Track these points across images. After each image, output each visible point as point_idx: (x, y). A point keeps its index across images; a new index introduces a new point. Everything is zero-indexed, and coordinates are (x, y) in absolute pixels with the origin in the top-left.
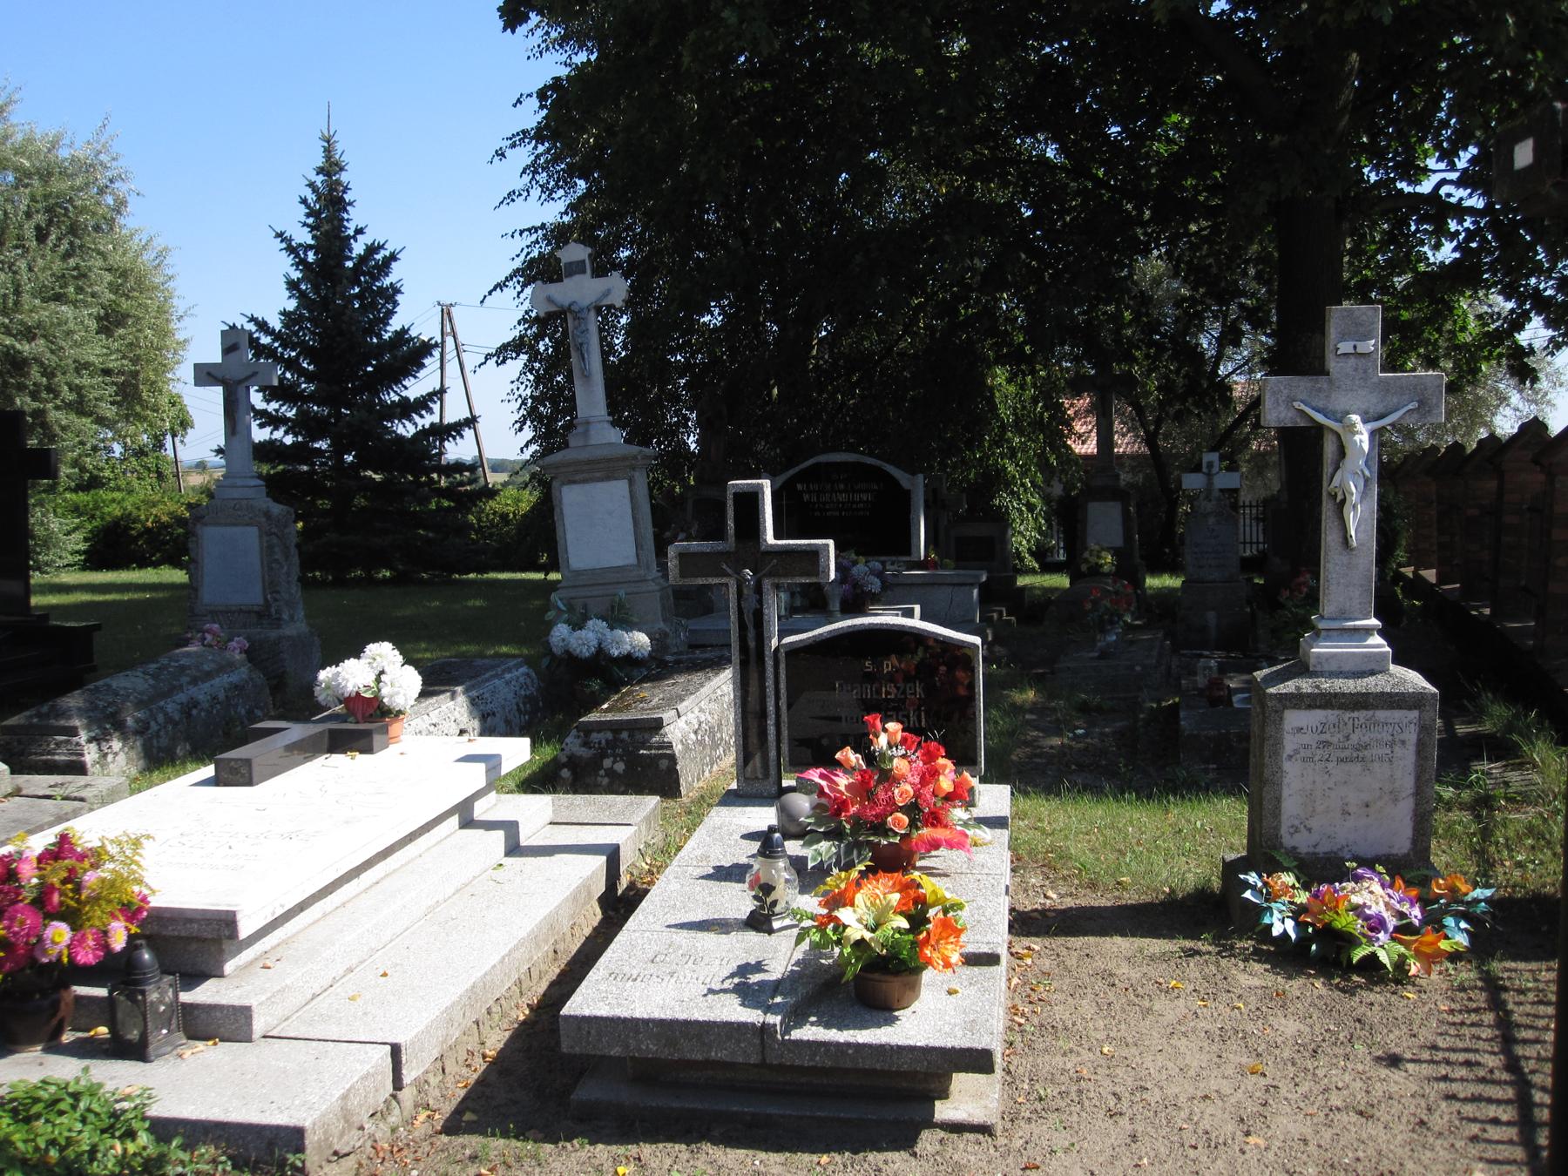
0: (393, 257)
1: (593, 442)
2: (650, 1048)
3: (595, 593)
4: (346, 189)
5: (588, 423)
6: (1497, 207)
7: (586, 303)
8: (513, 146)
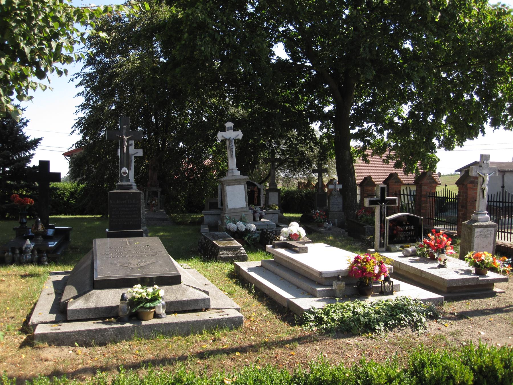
1: (234, 175)
2: (460, 284)
5: (232, 169)
7: (232, 138)
8: (76, 78)
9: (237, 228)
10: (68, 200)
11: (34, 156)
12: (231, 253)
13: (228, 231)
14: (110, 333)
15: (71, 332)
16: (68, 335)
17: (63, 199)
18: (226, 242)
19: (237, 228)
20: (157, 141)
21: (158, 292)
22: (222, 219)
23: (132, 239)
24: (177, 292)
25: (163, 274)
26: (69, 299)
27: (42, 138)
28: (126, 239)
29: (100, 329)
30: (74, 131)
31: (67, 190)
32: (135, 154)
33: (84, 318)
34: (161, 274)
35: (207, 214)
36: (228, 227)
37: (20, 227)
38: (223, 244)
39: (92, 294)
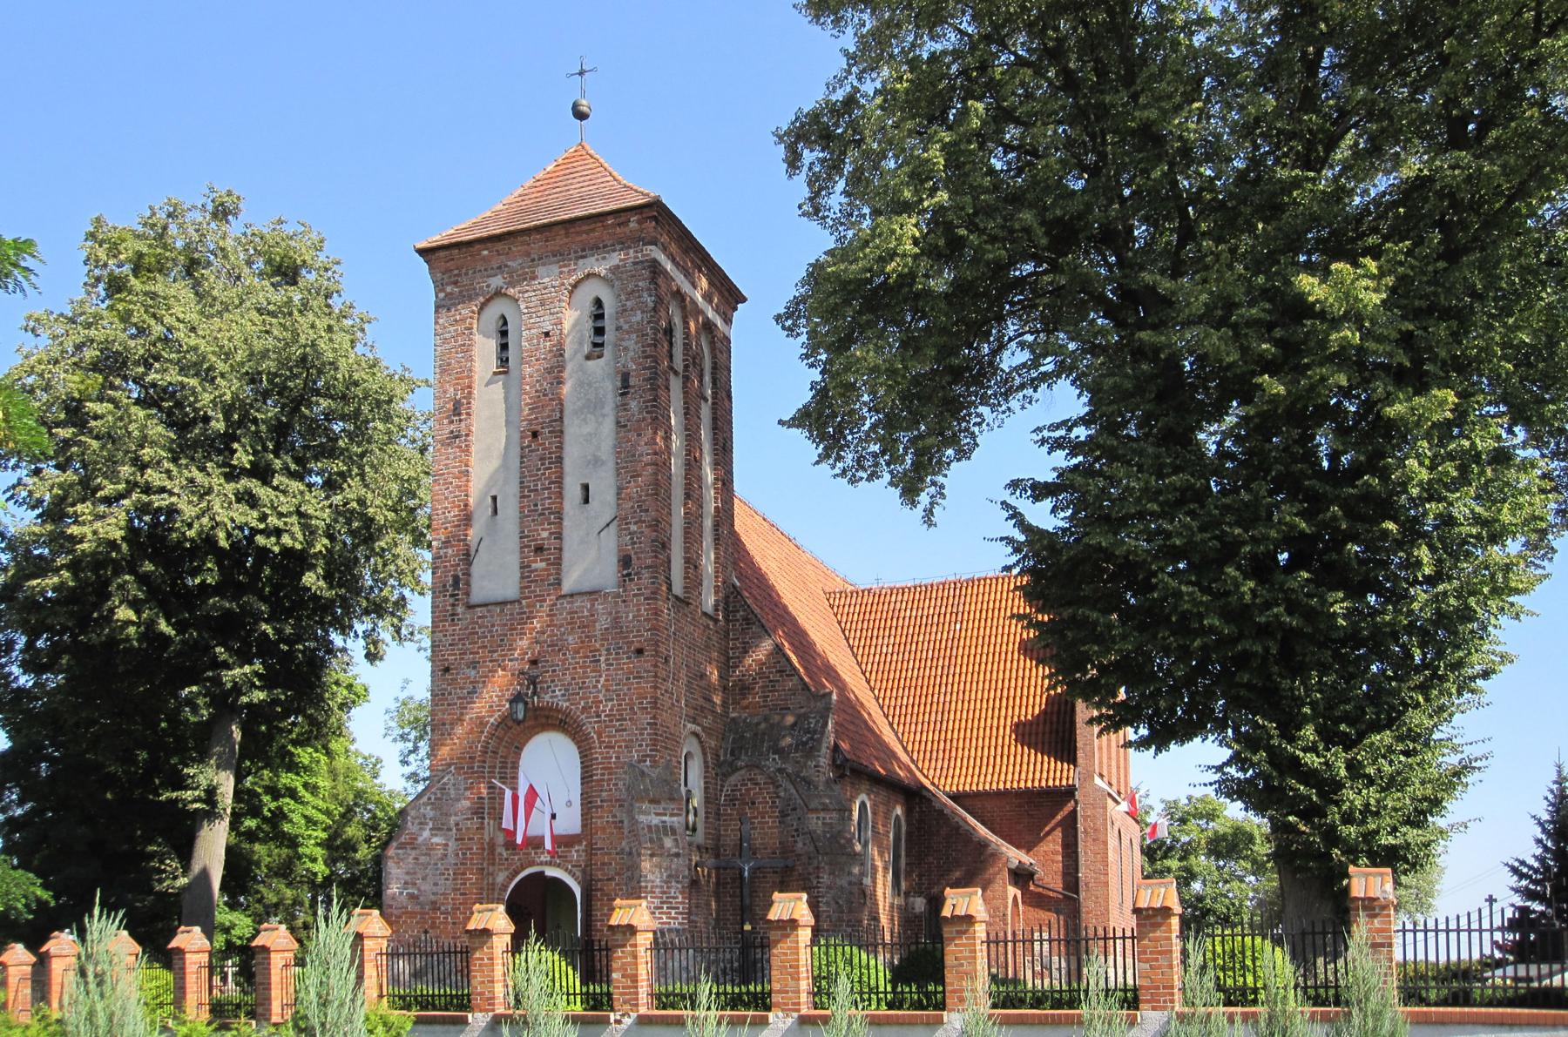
6: (1476, 112)
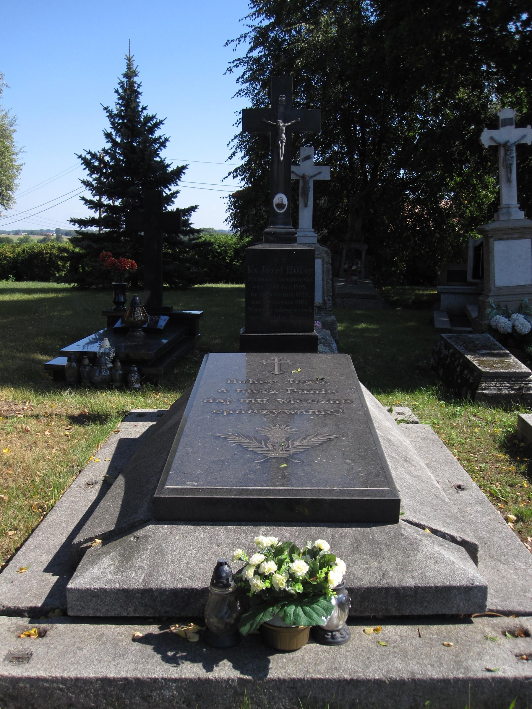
0: (161, 122)
1: (512, 218)
3: (508, 299)
4: (139, 86)
5: (509, 207)
7: (512, 141)
8: (236, 66)
9: (513, 326)
10: (232, 261)
11: (178, 195)
12: (507, 388)
13: (494, 331)
14: (167, 694)
15: (54, 680)
16: (46, 689)
17: (224, 259)
18: (494, 359)
19: (513, 326)
20: (363, 166)
21: (325, 570)
22: (481, 307)
23: (287, 358)
24: (386, 554)
25: (349, 492)
26: (92, 540)
27: (187, 165)
28: (275, 359)
29: (137, 680)
30: (234, 154)
31: (229, 245)
32: (315, 175)
33: (113, 614)
34: (341, 492)
35: (446, 293)
36: (493, 323)
37: (114, 310)
38: (490, 366)
39: (146, 537)
